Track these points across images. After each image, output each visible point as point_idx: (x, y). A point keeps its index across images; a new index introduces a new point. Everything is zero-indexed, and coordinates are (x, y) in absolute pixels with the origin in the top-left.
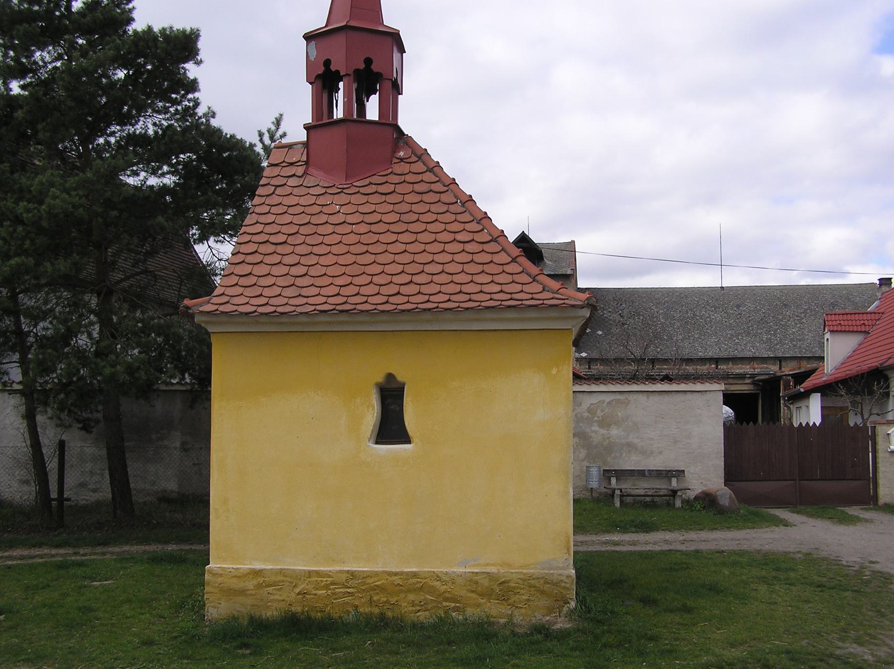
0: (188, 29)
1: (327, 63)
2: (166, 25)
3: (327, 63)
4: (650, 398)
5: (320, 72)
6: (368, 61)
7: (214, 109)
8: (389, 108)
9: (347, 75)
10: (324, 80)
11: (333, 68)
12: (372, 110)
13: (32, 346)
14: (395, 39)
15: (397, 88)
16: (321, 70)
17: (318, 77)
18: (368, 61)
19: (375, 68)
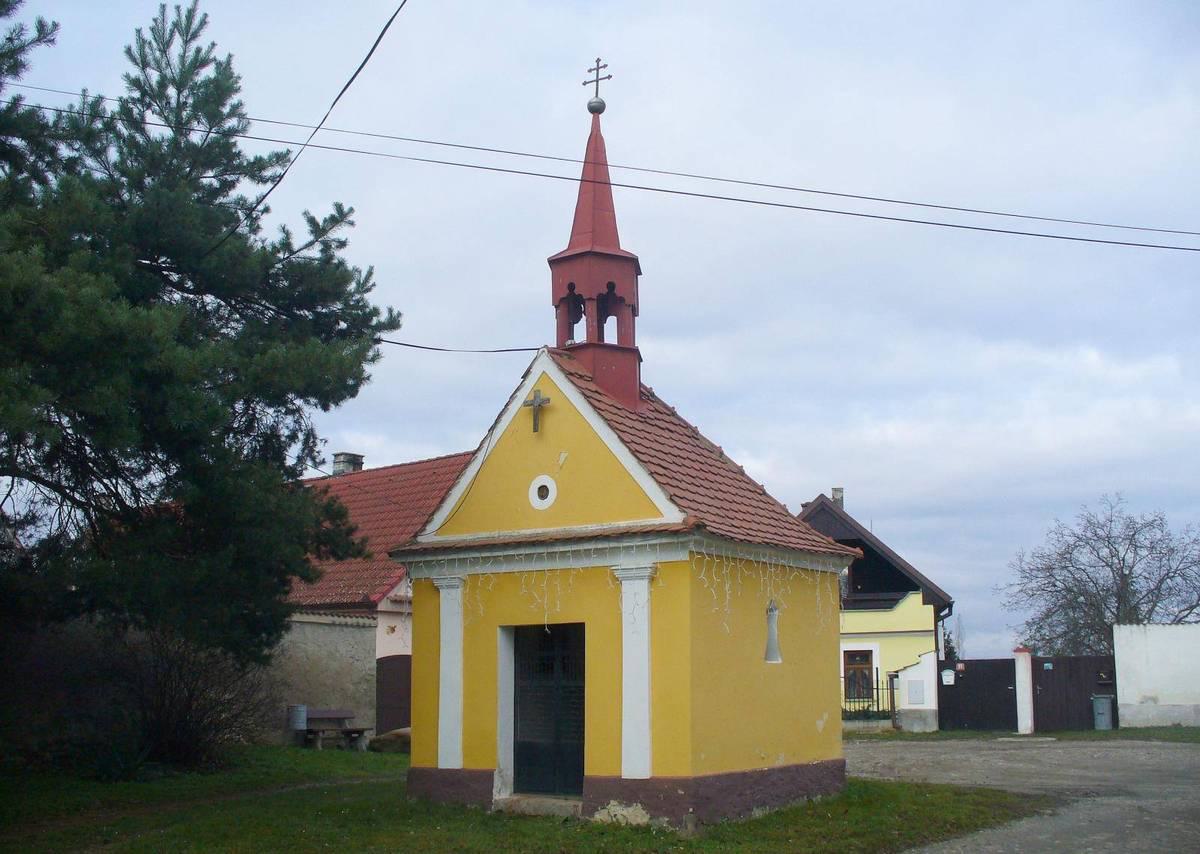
0: (332, 407)
1: (571, 287)
2: (359, 393)
3: (571, 287)
4: (671, 406)
5: (565, 295)
6: (611, 286)
7: (59, 36)
8: (626, 331)
9: (589, 299)
10: (569, 305)
11: (576, 292)
12: (611, 335)
13: (59, 418)
14: (632, 264)
15: (635, 312)
16: (565, 293)
17: (562, 300)
18: (611, 286)
19: (618, 292)
